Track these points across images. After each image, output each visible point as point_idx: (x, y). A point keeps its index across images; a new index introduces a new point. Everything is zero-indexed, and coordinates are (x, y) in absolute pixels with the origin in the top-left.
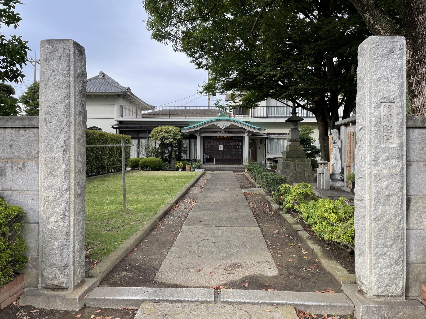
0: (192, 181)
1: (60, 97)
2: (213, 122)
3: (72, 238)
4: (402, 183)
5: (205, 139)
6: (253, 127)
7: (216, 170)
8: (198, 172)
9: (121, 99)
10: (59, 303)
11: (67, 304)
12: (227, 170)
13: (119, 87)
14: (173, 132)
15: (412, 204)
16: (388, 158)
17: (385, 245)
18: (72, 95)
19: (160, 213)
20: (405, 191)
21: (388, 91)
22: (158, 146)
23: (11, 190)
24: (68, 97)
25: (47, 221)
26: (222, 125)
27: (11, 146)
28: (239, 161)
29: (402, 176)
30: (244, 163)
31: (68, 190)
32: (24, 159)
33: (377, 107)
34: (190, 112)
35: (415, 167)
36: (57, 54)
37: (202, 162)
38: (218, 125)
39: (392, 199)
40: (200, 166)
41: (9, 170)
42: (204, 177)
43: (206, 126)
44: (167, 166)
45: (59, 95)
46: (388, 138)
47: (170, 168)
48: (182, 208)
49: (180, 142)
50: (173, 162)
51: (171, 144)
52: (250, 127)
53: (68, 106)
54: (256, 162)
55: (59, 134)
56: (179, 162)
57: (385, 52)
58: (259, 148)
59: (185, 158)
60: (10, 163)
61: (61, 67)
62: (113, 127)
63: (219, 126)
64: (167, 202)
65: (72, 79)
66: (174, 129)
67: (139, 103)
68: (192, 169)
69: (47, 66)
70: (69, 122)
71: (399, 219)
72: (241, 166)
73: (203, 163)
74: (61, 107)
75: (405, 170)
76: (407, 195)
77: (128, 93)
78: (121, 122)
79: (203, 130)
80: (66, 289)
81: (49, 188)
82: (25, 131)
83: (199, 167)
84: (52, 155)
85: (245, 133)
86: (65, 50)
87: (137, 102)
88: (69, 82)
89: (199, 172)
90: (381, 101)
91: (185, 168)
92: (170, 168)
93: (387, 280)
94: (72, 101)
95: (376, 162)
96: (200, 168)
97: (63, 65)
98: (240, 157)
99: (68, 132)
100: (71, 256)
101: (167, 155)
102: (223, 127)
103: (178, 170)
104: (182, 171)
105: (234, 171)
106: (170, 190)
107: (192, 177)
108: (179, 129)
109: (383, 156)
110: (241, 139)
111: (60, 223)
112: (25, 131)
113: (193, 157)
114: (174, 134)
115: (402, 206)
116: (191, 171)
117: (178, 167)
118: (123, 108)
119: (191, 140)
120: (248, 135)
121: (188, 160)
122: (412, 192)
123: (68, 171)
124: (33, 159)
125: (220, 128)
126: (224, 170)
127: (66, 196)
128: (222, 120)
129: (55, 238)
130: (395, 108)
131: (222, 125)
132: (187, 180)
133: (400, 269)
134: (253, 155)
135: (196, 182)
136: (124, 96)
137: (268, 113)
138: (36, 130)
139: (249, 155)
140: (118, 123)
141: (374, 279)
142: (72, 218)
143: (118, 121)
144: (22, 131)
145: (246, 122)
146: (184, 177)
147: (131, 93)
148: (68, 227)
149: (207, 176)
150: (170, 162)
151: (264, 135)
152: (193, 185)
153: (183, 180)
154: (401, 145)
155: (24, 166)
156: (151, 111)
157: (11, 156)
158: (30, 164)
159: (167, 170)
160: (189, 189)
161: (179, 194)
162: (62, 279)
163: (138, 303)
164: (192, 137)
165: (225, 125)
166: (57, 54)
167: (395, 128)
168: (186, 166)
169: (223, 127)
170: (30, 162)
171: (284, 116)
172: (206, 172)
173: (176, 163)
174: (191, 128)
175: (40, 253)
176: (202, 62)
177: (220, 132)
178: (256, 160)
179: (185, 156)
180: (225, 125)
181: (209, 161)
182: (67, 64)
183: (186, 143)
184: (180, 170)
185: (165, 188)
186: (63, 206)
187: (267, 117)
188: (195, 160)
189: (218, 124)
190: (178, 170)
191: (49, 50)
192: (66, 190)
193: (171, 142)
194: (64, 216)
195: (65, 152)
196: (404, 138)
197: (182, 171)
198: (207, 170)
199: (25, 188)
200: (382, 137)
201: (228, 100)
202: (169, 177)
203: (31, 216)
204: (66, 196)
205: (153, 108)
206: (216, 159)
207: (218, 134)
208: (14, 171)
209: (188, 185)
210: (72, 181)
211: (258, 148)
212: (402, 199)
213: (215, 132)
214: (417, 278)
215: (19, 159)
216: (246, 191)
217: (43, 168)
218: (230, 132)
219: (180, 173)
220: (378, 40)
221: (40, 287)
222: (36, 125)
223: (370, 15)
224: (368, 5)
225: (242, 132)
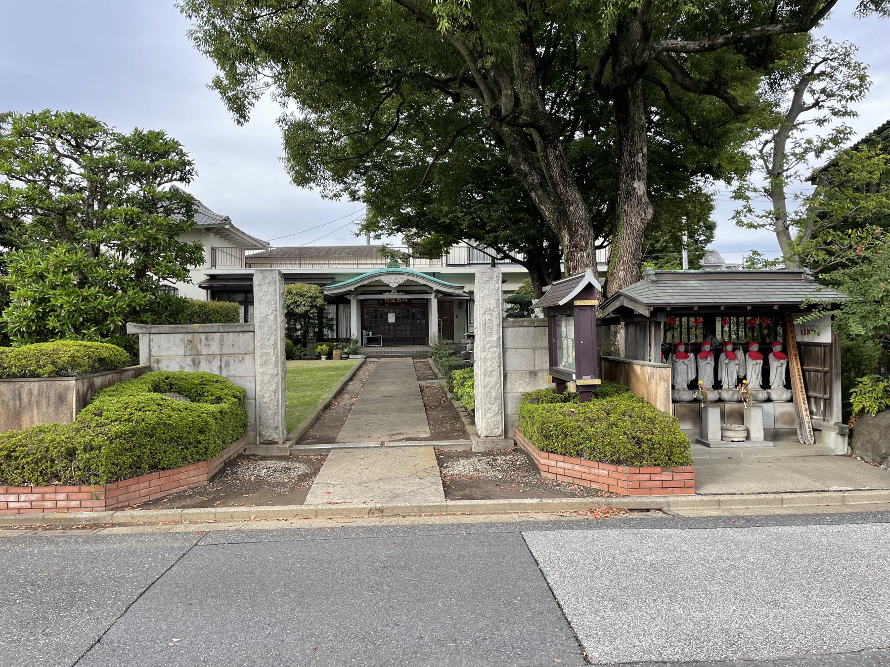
0: (348, 374)
1: (270, 311)
2: (377, 276)
3: (280, 408)
4: (500, 362)
5: (362, 304)
6: (443, 284)
7: (384, 357)
8: (354, 361)
9: (212, 235)
10: (275, 451)
11: (280, 452)
12: (402, 356)
13: (209, 215)
14: (309, 294)
15: (508, 376)
16: (491, 347)
17: (490, 403)
18: (278, 309)
19: (321, 406)
20: (502, 368)
21: (490, 304)
23: (234, 376)
24: (276, 310)
25: (263, 397)
26: (393, 281)
28: (422, 338)
29: (500, 359)
30: (431, 344)
31: (277, 375)
33: (484, 314)
34: (334, 253)
35: (509, 353)
36: (267, 281)
37: (359, 344)
39: (494, 373)
40: (357, 350)
41: (232, 362)
42: (365, 367)
43: (365, 283)
44: (301, 352)
46: (491, 335)
47: (305, 355)
48: (343, 403)
49: (321, 310)
50: (310, 345)
51: (306, 315)
52: (439, 283)
53: (276, 316)
54: (451, 341)
55: (270, 336)
56: (321, 345)
59: (330, 337)
60: (232, 357)
61: (270, 290)
62: (200, 287)
64: (324, 397)
65: (278, 298)
66: (312, 289)
67: (242, 240)
68: (343, 356)
70: (277, 327)
71: (498, 386)
72: (425, 349)
73: (362, 345)
74: (272, 317)
77: (227, 227)
78: (213, 277)
79: (362, 290)
80: (277, 443)
81: (263, 374)
83: (355, 352)
84: (265, 351)
85: (431, 293)
86: (273, 278)
87: (238, 237)
88: (276, 300)
89: (355, 360)
91: (332, 354)
92: (305, 355)
93: (492, 426)
94: (278, 313)
95: (484, 350)
96: (357, 353)
97: (272, 288)
98: (424, 332)
99: (276, 334)
100: (280, 420)
101: (299, 333)
103: (320, 358)
104: (327, 359)
105: (413, 357)
106: (321, 385)
107: (346, 368)
108: (319, 288)
109: (488, 346)
110: (426, 303)
111: (273, 398)
113: (343, 335)
114: (311, 297)
115: (500, 378)
116: (341, 358)
117: (319, 353)
118: (217, 252)
119: (340, 305)
120: (436, 297)
121: (337, 340)
122: (508, 369)
123: (277, 361)
125: (388, 285)
126: (398, 356)
127: (276, 379)
128: (392, 273)
129: (269, 408)
130: (495, 314)
131: (393, 282)
132: (341, 372)
133: (500, 418)
134: (446, 330)
135: (354, 375)
136: (219, 230)
137: (469, 258)
138: (252, 333)
139: (439, 329)
140: (209, 278)
141: (484, 425)
142: (280, 394)
143: (207, 275)
144: (241, 334)
145: (434, 275)
146: (336, 369)
147: (232, 226)
148: (278, 400)
149: (370, 367)
150: (305, 345)
151: (465, 294)
152: (351, 379)
153: (335, 373)
154: (499, 338)
155: (243, 359)
156: (262, 251)
157: (234, 352)
159: (301, 359)
160: (346, 384)
161: (335, 388)
162: (275, 436)
163: (329, 450)
164: (341, 300)
165: (396, 281)
166: (267, 281)
167: (495, 328)
168: (334, 352)
169: (394, 285)
170: (248, 356)
172: (368, 359)
173: (317, 347)
174: (340, 287)
175: (258, 420)
176: (358, 191)
177: (390, 292)
178: (451, 337)
179: (329, 334)
180: (396, 281)
181: (371, 341)
183: (331, 310)
184: (323, 358)
185: (313, 383)
186: (274, 385)
187: (469, 264)
188: (348, 340)
189: (386, 280)
190: (320, 358)
191: (261, 278)
192: (276, 375)
193: (306, 312)
194: (275, 392)
195: (275, 348)
197: (327, 359)
198: (368, 357)
199: (244, 375)
202: (311, 370)
203: (251, 394)
204: (276, 379)
205: (265, 245)
206: (384, 337)
207: (386, 296)
208: (236, 362)
209: (344, 379)
210: (280, 368)
212: (500, 373)
213: (381, 292)
214: (513, 424)
216: (423, 383)
217: (258, 361)
218: (407, 293)
219: (323, 362)
221: (258, 443)
222: (252, 330)
223: (536, 195)
224: (532, 184)
225: (427, 293)
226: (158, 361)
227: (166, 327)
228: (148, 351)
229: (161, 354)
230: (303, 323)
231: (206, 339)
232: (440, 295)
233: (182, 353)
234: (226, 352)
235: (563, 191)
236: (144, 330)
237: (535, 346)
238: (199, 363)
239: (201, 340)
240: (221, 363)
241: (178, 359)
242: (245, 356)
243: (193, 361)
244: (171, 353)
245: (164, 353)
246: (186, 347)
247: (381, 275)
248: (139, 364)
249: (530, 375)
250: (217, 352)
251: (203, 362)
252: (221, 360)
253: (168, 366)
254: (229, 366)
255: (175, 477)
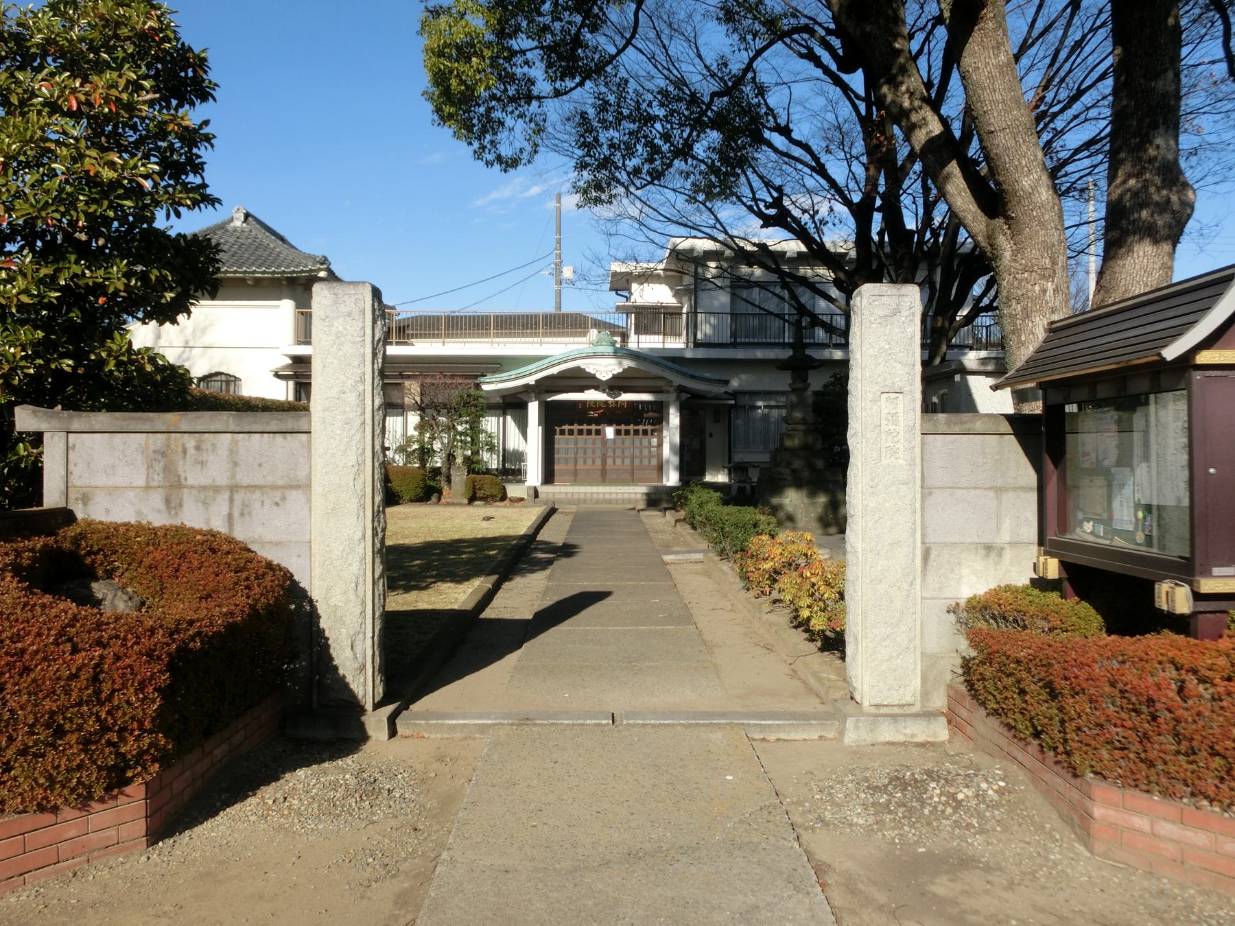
4: (914, 523)
15: (932, 557)
22: (412, 432)
27: (260, 465)
32: (283, 487)
38: (590, 370)
41: (257, 505)
45: (348, 378)
57: (887, 312)
58: (711, 435)
62: (277, 375)
63: (593, 372)
69: (326, 329)
70: (364, 423)
75: (918, 505)
76: (923, 543)
82: (285, 438)
85: (668, 392)
90: (882, 390)
102: (604, 374)
112: (285, 438)
124: (298, 487)
138: (304, 436)
144: (279, 437)
155: (284, 498)
158: (295, 497)
166: (343, 309)
171: (781, 341)
182: (360, 325)
187: (733, 345)
196: (918, 451)
200: (883, 450)
201: (616, 290)
208: (266, 507)
211: (708, 435)
215: (275, 488)
220: (876, 292)
222: (305, 429)
226: (85, 499)
227: (102, 419)
228: (63, 473)
229: (93, 483)
230: (446, 441)
231: (198, 448)
232: (685, 396)
233: (141, 482)
234: (245, 482)
235: (1011, 143)
236: (55, 424)
237: (999, 483)
238: (181, 505)
239: (185, 452)
240: (231, 508)
241: (131, 494)
242: (288, 493)
243: (168, 501)
244: (117, 480)
245: (100, 480)
246: (150, 467)
247: (583, 358)
248: (42, 505)
249: (987, 555)
250: (223, 480)
251: (188, 499)
252: (231, 500)
253: (107, 511)
254: (250, 514)
255: (43, 836)
